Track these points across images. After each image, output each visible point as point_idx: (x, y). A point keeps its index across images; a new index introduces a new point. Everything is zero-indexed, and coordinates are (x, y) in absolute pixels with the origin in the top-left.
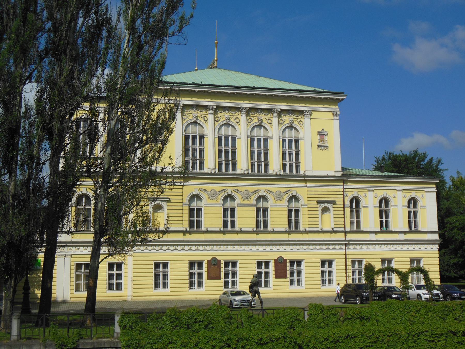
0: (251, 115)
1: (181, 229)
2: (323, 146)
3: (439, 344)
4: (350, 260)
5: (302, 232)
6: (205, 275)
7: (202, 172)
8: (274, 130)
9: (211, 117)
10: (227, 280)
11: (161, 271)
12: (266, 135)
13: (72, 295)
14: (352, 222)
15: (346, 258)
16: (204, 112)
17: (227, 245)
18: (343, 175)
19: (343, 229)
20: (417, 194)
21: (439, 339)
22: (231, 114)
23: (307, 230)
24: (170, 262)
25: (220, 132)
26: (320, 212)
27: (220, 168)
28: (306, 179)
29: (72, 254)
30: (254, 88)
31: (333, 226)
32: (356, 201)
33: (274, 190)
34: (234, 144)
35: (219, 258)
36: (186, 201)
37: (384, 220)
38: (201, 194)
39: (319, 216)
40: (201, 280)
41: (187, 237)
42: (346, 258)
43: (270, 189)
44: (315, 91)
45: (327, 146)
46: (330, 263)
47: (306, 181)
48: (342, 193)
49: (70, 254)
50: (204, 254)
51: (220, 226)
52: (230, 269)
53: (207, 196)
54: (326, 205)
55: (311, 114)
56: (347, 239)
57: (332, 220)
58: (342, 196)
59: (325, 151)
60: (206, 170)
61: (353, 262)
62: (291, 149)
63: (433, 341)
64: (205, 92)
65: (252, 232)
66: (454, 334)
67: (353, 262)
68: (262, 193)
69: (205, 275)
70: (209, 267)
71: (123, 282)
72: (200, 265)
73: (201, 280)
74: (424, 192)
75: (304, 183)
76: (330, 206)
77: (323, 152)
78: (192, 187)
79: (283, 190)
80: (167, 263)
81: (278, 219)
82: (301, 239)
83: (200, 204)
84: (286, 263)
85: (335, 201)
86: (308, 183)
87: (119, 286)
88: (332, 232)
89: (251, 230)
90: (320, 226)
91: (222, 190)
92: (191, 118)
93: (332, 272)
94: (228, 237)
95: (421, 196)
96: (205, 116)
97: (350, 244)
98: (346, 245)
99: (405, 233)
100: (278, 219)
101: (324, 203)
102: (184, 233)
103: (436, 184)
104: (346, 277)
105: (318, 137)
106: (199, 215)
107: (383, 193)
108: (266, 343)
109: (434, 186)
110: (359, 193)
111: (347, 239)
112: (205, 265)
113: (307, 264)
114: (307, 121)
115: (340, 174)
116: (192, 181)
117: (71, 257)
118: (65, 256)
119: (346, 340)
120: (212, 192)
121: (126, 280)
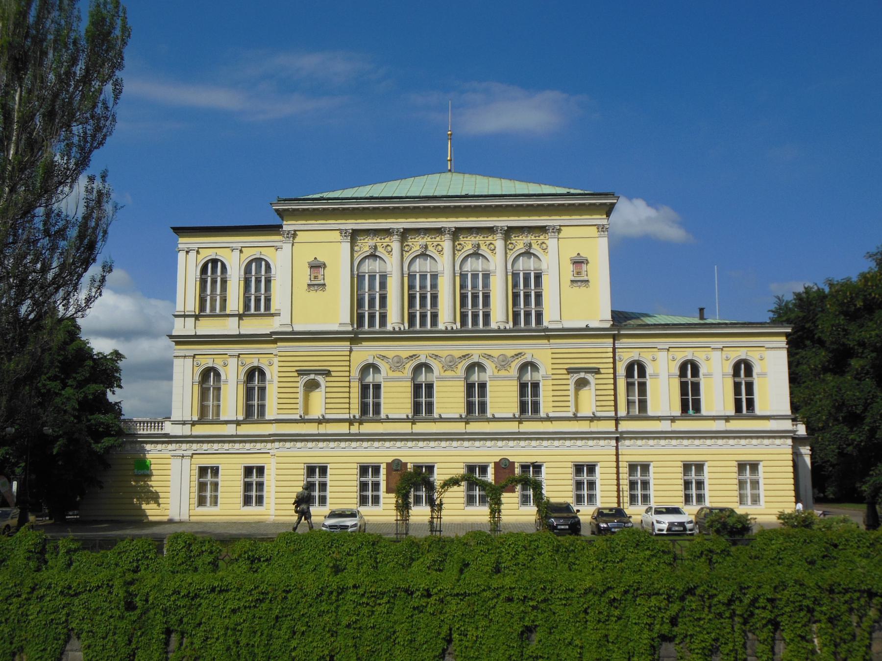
0: (462, 239)
1: (347, 416)
2: (580, 282)
3: (379, 609)
4: (626, 464)
5: (542, 420)
6: (383, 486)
7: (540, 327)
8: (496, 260)
9: (499, 244)
10: (689, 492)
11: (585, 477)
12: (486, 267)
13: (192, 512)
14: (629, 403)
15: (617, 461)
16: (490, 238)
17: (452, 440)
18: (612, 325)
19: (613, 414)
20: (749, 353)
21: (378, 601)
22: (429, 239)
23: (551, 415)
24: (436, 466)
25: (412, 269)
26: (572, 387)
27: (360, 323)
28: (549, 335)
29: (193, 454)
30: (467, 196)
31: (594, 409)
32: (636, 369)
33: (495, 353)
34: (486, 285)
35: (511, 459)
36: (355, 373)
37: (744, 397)
38: (378, 362)
39: (572, 393)
40: (702, 492)
41: (355, 429)
42: (617, 461)
43: (383, 354)
44: (568, 194)
45: (324, 285)
46: (591, 469)
47: (548, 337)
48: (611, 355)
49: (190, 453)
50: (382, 454)
51: (462, 411)
52: (638, 477)
53: (388, 366)
54: (582, 375)
55: (559, 231)
56: (620, 430)
57: (594, 398)
58: (611, 360)
59: (320, 293)
60: (493, 325)
61: (632, 467)
62: (527, 290)
63: (368, 604)
64: (455, 207)
65: (460, 419)
66: (409, 592)
67: (632, 467)
68: (423, 360)
69: (383, 486)
70: (388, 474)
71: (265, 494)
72: (376, 470)
73: (702, 492)
74: (709, 349)
75: (546, 341)
76: (589, 377)
77: (580, 291)
78: (364, 353)
79: (510, 353)
80: (433, 467)
81: (502, 398)
82: (541, 430)
83: (379, 378)
84: (514, 468)
85: (599, 369)
86: (552, 341)
87: (260, 500)
88: (593, 418)
89: (457, 416)
90: (572, 409)
91: (411, 357)
92: (367, 249)
93: (758, 482)
94: (420, 428)
95: (759, 357)
96: (388, 245)
97: (625, 439)
98: (617, 439)
99: (727, 419)
100: (502, 398)
101: (579, 372)
102: (351, 422)
103: (787, 335)
104: (618, 491)
105: (571, 267)
106: (377, 395)
107: (686, 354)
108: (76, 594)
109: (784, 339)
110: (749, 353)
111: (620, 430)
112: (383, 471)
113: (768, 469)
114: (551, 242)
115: (350, 328)
116: (364, 344)
117: (192, 457)
118: (183, 456)
119: (212, 596)
120: (501, 358)
121: (269, 492)
